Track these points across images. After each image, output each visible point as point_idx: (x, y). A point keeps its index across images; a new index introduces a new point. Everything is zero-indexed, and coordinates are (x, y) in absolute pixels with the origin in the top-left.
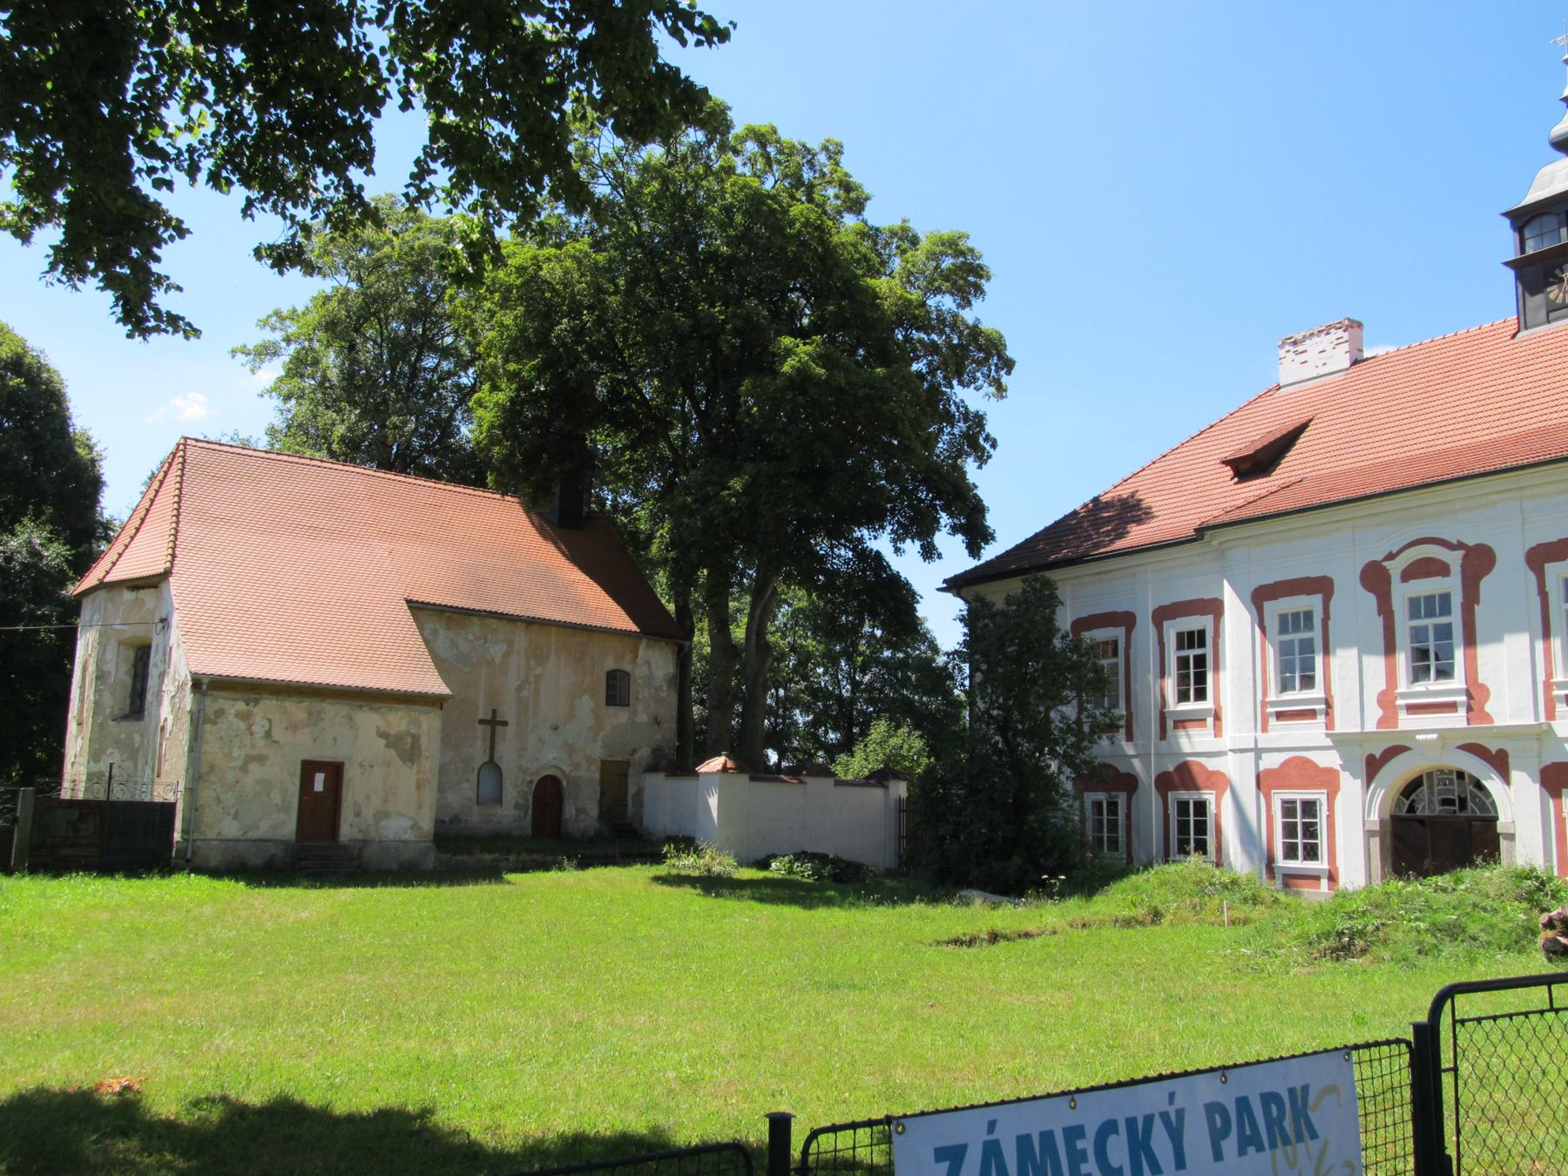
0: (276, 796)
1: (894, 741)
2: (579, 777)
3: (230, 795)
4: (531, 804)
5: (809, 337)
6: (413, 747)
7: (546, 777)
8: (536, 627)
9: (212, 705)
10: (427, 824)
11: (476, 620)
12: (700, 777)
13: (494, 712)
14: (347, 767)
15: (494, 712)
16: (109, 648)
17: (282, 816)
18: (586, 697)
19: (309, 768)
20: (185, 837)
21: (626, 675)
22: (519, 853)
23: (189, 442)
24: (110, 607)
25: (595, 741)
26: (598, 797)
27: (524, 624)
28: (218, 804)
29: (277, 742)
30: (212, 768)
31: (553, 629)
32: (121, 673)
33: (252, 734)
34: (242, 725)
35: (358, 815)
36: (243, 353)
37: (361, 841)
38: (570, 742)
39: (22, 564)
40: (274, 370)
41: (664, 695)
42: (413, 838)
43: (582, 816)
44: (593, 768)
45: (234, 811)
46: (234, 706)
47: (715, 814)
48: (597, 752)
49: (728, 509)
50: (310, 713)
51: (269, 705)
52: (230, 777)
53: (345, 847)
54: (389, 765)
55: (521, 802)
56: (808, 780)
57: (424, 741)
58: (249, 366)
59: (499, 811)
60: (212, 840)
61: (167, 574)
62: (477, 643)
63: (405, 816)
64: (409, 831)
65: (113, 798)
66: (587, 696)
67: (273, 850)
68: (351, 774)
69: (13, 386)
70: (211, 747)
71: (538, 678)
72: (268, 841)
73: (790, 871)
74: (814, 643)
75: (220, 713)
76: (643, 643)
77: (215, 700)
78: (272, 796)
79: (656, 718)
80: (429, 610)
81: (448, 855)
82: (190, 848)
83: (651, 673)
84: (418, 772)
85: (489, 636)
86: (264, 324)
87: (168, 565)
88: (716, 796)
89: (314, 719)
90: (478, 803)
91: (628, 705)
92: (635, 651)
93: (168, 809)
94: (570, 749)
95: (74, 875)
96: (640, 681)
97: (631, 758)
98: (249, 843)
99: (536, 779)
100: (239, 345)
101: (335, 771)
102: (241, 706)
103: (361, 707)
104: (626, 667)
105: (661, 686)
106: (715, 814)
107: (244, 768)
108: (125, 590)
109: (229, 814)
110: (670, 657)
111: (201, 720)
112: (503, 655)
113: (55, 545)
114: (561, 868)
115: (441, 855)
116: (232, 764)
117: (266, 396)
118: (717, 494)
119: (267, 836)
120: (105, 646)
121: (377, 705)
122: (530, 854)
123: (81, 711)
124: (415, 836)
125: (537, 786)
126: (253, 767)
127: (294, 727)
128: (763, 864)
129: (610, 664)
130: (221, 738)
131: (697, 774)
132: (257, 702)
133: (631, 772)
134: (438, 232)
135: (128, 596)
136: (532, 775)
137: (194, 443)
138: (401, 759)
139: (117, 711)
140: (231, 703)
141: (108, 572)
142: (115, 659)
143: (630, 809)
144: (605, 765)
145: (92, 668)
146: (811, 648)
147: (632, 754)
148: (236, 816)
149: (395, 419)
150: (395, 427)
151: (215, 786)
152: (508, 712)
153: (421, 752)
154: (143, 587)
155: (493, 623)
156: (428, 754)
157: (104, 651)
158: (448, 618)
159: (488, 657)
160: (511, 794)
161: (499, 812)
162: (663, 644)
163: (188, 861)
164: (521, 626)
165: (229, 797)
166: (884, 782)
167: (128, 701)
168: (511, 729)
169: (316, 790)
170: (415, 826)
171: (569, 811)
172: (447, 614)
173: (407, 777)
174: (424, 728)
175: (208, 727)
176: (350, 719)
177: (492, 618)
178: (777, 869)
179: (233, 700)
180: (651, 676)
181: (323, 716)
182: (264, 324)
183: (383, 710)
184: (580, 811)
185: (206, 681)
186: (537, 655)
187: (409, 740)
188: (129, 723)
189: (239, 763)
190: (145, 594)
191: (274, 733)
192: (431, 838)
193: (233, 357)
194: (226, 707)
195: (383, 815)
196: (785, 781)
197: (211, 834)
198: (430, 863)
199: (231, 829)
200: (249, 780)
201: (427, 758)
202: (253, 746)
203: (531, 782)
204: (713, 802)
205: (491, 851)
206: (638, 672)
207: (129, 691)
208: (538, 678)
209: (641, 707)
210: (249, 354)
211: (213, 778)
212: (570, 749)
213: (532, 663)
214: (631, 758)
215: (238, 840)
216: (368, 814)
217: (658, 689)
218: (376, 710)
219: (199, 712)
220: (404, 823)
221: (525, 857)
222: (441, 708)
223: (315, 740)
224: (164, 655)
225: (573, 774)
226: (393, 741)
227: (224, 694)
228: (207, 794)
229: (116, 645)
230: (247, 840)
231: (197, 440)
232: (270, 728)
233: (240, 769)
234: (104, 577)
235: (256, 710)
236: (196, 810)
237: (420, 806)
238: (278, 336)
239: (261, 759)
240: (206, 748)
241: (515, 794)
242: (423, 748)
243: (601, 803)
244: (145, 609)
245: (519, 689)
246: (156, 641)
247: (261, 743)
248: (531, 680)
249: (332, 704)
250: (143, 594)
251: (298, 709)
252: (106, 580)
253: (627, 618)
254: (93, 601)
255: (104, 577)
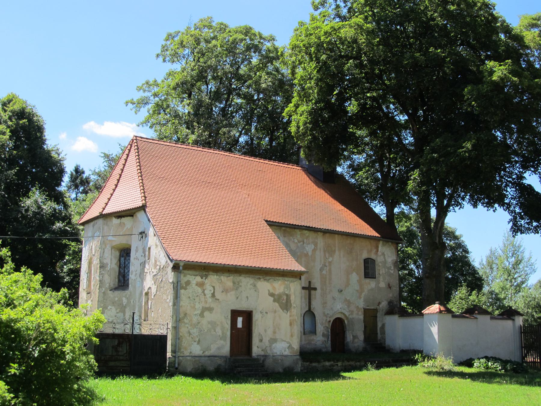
0: (219, 332)
1: (471, 298)
2: (353, 318)
3: (195, 330)
4: (330, 334)
5: (504, 61)
6: (287, 302)
7: (336, 319)
8: (327, 235)
9: (184, 279)
10: (296, 346)
11: (298, 231)
12: (424, 315)
13: (310, 282)
14: (254, 313)
15: (310, 282)
16: (106, 250)
17: (222, 342)
18: (354, 274)
19: (235, 314)
20: (174, 355)
21: (373, 261)
22: (343, 361)
23: (138, 138)
24: (106, 227)
25: (360, 298)
26: (363, 329)
27: (322, 233)
28: (189, 336)
29: (218, 300)
30: (186, 314)
31: (336, 236)
32: (112, 263)
33: (205, 295)
34: (200, 290)
35: (261, 341)
36: (131, 103)
37: (263, 356)
38: (348, 299)
39: (33, 212)
40: (144, 112)
41: (392, 272)
42: (289, 354)
43: (356, 340)
44: (360, 313)
45: (197, 340)
46: (195, 279)
47: (436, 337)
48: (361, 304)
49: (463, 159)
50: (234, 283)
51: (213, 278)
52: (195, 319)
53: (256, 360)
54: (275, 312)
55: (325, 333)
56: (478, 316)
57: (292, 298)
58: (134, 110)
59: (313, 337)
60: (187, 356)
61: (143, 208)
62: (299, 244)
63: (285, 341)
64: (287, 350)
65: (135, 333)
66: (355, 273)
67: (219, 362)
68: (256, 317)
69: (22, 124)
70: (184, 302)
71: (330, 263)
72: (216, 356)
73: (487, 368)
74: (411, 249)
75: (188, 283)
76: (381, 242)
77: (185, 276)
78: (217, 331)
79: (389, 285)
80: (277, 226)
81: (308, 364)
82: (177, 361)
83: (385, 260)
84: (290, 316)
85: (305, 240)
86: (139, 89)
87: (144, 202)
88: (436, 327)
89: (236, 286)
90: (304, 334)
91: (375, 278)
92: (377, 248)
93: (163, 339)
94: (348, 303)
95: (121, 377)
96: (380, 264)
97: (378, 307)
98: (207, 358)
99: (332, 320)
100: (129, 99)
101: (248, 316)
102: (198, 279)
103: (260, 278)
104: (373, 256)
105: (391, 267)
106: (436, 337)
107: (202, 315)
108: (114, 218)
109: (195, 341)
110: (394, 250)
111: (179, 288)
112: (313, 251)
113: (49, 202)
114: (368, 370)
115: (305, 363)
116: (196, 312)
117: (141, 126)
118: (455, 151)
119: (216, 354)
120: (104, 249)
121: (268, 278)
122: (349, 362)
123: (89, 285)
124: (290, 353)
125: (332, 323)
126: (206, 314)
127: (226, 291)
128: (469, 363)
129: (365, 256)
130: (189, 297)
131: (422, 315)
132: (206, 276)
133: (378, 315)
134: (241, 32)
135: (115, 221)
136: (330, 317)
137: (140, 139)
138: (281, 308)
139: (112, 286)
140: (193, 277)
141: (104, 209)
142: (110, 256)
143: (379, 336)
144: (366, 311)
145: (96, 262)
146: (410, 252)
147: (378, 305)
148: (199, 342)
149: (224, 130)
150: (224, 133)
151: (187, 325)
152: (316, 283)
153: (291, 304)
154: (124, 216)
155: (306, 232)
156: (294, 305)
157: (104, 252)
158: (284, 230)
159: (305, 252)
160: (320, 329)
161: (315, 338)
162: (390, 244)
163: (177, 369)
164: (320, 234)
165: (195, 332)
166: (512, 317)
167: (117, 280)
168: (319, 291)
169: (238, 327)
170: (290, 347)
171: (349, 337)
172: (284, 228)
173: (285, 318)
174: (292, 290)
175: (182, 291)
176: (255, 286)
177: (306, 230)
178: (478, 367)
179: (194, 275)
180: (385, 262)
181: (240, 284)
182: (139, 89)
183: (271, 280)
184: (355, 337)
185: (182, 264)
186: (329, 251)
187: (285, 297)
188: (119, 292)
189: (199, 312)
190: (126, 221)
191: (216, 294)
192: (299, 354)
193: (127, 105)
194: (191, 279)
195: (273, 341)
196: (467, 317)
197: (187, 353)
198: (298, 368)
199: (196, 350)
200: (204, 322)
201: (294, 307)
202: (206, 302)
203: (330, 321)
204: (435, 330)
205: (329, 360)
206: (379, 260)
207: (117, 274)
208: (330, 263)
209: (381, 279)
210: (135, 104)
211: (186, 321)
212: (348, 303)
213: (327, 255)
214: (378, 307)
215: (201, 356)
216: (266, 340)
217: (389, 268)
218: (268, 281)
219: (177, 282)
220: (285, 345)
221: (346, 363)
222: (300, 279)
223: (237, 298)
224: (144, 252)
225: (351, 317)
226: (277, 298)
227: (190, 272)
228: (183, 330)
229: (110, 249)
230: (205, 356)
231: (142, 138)
232: (214, 292)
233: (200, 315)
234: (102, 211)
235: (206, 281)
236: (179, 339)
237: (292, 336)
238: (147, 94)
239: (210, 309)
240: (182, 303)
241: (322, 328)
242: (292, 302)
243: (365, 332)
244: (125, 229)
245: (321, 270)
246: (135, 244)
247: (210, 300)
248: (327, 264)
249: (245, 277)
250: (124, 220)
251: (227, 280)
252: (104, 213)
253: (372, 229)
254: (93, 226)
255: (102, 211)
